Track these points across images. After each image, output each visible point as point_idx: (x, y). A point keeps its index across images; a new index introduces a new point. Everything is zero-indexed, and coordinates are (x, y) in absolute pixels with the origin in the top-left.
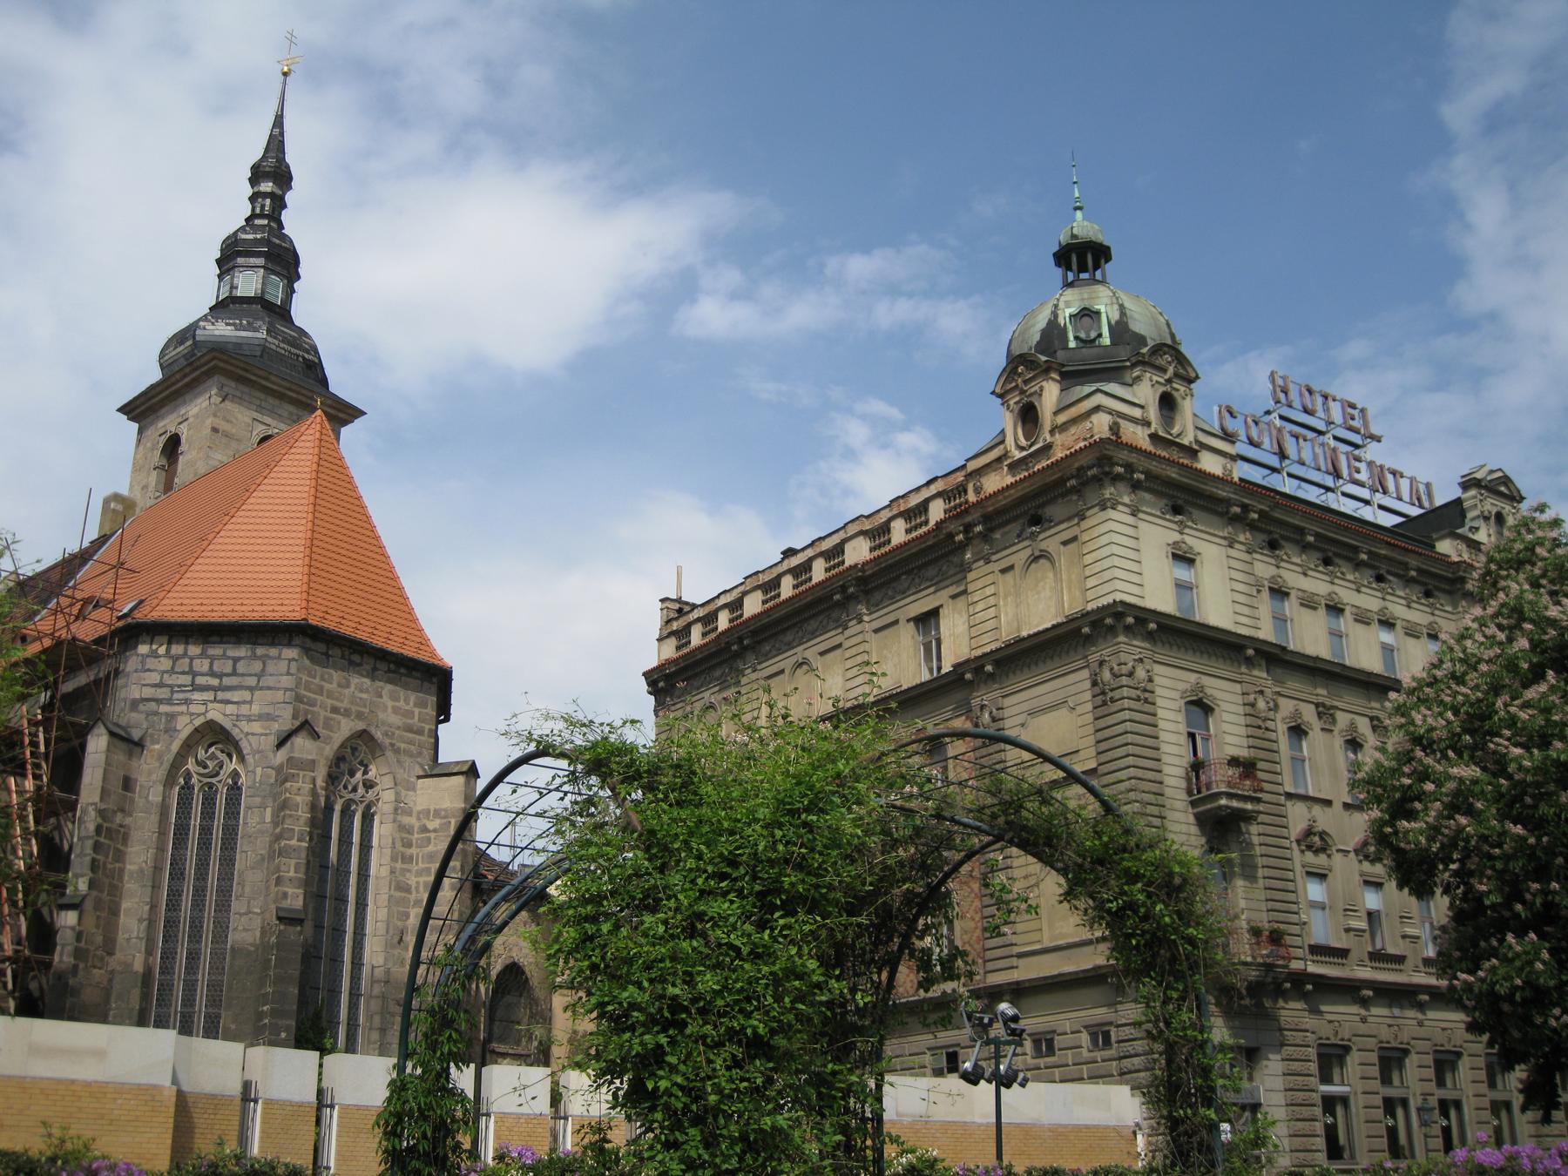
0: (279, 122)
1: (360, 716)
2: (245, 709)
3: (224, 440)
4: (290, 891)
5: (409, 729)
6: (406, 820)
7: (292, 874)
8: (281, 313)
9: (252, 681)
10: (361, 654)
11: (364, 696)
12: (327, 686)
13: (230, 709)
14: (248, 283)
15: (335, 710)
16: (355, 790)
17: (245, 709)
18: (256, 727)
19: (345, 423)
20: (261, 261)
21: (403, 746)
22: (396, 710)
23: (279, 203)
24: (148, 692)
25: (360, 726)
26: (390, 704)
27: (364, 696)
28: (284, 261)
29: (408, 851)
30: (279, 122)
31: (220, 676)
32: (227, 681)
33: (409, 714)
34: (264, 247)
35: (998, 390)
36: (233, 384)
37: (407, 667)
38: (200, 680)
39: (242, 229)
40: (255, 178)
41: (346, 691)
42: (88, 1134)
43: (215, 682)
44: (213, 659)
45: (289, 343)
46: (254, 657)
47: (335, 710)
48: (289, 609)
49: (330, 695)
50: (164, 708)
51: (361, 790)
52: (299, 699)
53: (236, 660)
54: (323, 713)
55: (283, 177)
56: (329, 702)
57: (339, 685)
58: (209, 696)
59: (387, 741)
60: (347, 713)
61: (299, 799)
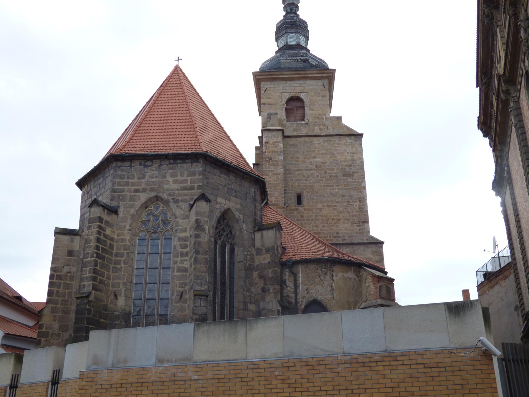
1: (152, 190)
3: (269, 106)
4: (86, 283)
7: (88, 275)
10: (151, 160)
11: (154, 180)
12: (131, 181)
15: (136, 191)
21: (180, 198)
22: (175, 182)
26: (171, 180)
27: (154, 180)
34: (292, 25)
36: (269, 83)
37: (180, 159)
41: (143, 180)
45: (292, 56)
49: (133, 184)
54: (129, 194)
56: (133, 188)
57: (139, 178)
59: (170, 198)
60: (144, 190)
61: (92, 237)
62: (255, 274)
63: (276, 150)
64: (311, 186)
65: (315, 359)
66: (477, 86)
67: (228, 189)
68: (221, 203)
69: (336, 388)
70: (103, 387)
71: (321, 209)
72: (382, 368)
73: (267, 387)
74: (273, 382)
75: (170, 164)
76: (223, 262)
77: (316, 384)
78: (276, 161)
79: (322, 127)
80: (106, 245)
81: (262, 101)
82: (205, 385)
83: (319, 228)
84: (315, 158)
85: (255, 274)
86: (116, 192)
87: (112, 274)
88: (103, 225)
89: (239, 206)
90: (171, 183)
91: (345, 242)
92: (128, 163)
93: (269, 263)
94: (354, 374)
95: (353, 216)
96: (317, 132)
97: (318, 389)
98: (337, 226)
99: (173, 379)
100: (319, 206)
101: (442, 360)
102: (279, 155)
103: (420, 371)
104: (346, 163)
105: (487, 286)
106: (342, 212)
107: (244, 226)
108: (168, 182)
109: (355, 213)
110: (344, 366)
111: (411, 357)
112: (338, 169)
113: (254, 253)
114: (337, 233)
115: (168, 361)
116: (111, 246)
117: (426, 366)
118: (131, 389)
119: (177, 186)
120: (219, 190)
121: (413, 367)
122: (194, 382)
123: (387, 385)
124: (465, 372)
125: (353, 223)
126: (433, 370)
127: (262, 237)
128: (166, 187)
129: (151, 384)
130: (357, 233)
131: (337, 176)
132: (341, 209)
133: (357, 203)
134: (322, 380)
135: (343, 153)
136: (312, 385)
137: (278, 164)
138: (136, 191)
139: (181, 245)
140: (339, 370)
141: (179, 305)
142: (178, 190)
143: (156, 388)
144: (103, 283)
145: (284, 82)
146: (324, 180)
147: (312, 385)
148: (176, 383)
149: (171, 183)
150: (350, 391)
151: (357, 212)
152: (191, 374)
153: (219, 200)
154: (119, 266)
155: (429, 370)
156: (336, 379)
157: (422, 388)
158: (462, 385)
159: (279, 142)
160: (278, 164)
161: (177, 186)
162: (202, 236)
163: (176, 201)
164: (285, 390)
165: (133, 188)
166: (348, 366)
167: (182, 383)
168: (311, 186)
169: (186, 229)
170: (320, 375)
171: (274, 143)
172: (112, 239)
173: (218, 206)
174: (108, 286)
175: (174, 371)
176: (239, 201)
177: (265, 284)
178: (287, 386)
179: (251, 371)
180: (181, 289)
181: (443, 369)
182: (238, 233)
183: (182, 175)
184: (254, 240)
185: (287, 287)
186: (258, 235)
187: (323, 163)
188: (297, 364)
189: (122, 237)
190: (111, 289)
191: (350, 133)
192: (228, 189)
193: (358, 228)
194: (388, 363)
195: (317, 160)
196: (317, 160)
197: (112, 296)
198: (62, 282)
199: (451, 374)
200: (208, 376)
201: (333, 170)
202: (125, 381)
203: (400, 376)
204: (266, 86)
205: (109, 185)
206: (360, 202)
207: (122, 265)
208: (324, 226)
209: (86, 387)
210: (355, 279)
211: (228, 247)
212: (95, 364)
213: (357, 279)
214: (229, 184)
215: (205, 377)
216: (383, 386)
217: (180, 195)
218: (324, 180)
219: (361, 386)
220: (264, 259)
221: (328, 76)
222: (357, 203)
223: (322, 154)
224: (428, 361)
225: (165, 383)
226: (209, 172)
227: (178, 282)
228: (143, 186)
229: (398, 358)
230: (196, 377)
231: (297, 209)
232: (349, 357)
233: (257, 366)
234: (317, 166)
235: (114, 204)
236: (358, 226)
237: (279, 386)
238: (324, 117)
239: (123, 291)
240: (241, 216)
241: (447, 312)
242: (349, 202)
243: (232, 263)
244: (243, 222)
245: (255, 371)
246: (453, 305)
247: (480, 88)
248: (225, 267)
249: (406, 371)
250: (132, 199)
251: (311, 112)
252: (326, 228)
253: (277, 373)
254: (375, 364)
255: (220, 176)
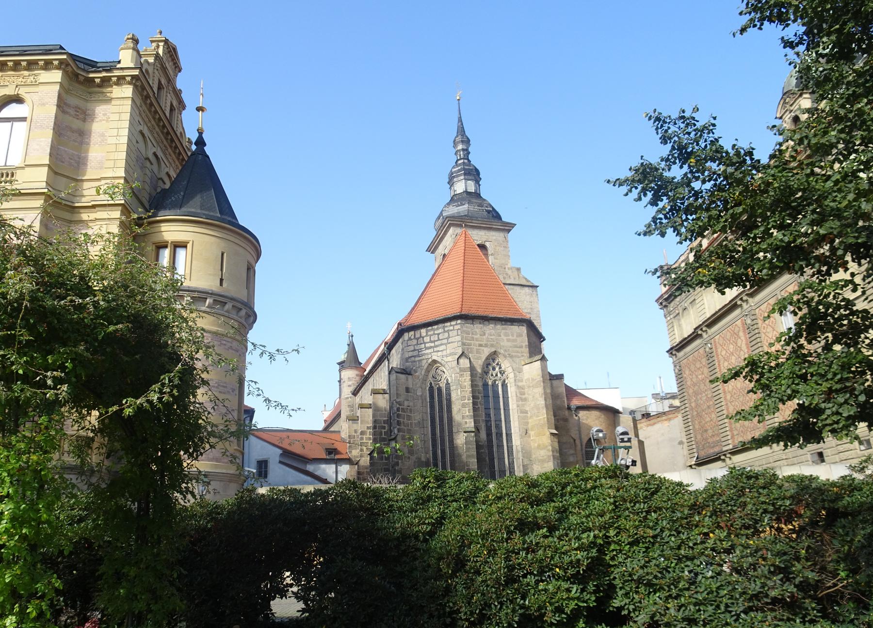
0: (460, 120)
1: (492, 346)
2: (444, 353)
5: (516, 347)
6: (520, 384)
8: (477, 195)
9: (445, 341)
12: (475, 337)
13: (440, 354)
14: (460, 187)
15: (480, 345)
16: (497, 375)
17: (444, 353)
18: (449, 359)
19: (509, 231)
20: (462, 177)
22: (508, 340)
23: (467, 152)
24: (411, 354)
25: (493, 350)
26: (505, 338)
28: (473, 174)
29: (524, 397)
30: (460, 120)
31: (434, 341)
32: (436, 343)
33: (515, 341)
35: (778, 116)
38: (427, 345)
39: (454, 167)
40: (455, 144)
42: (789, 449)
43: (432, 345)
44: (430, 336)
46: (445, 331)
47: (480, 345)
48: (455, 310)
50: (417, 359)
51: (499, 375)
52: (463, 344)
53: (438, 334)
55: (467, 141)
58: (432, 350)
60: (486, 346)
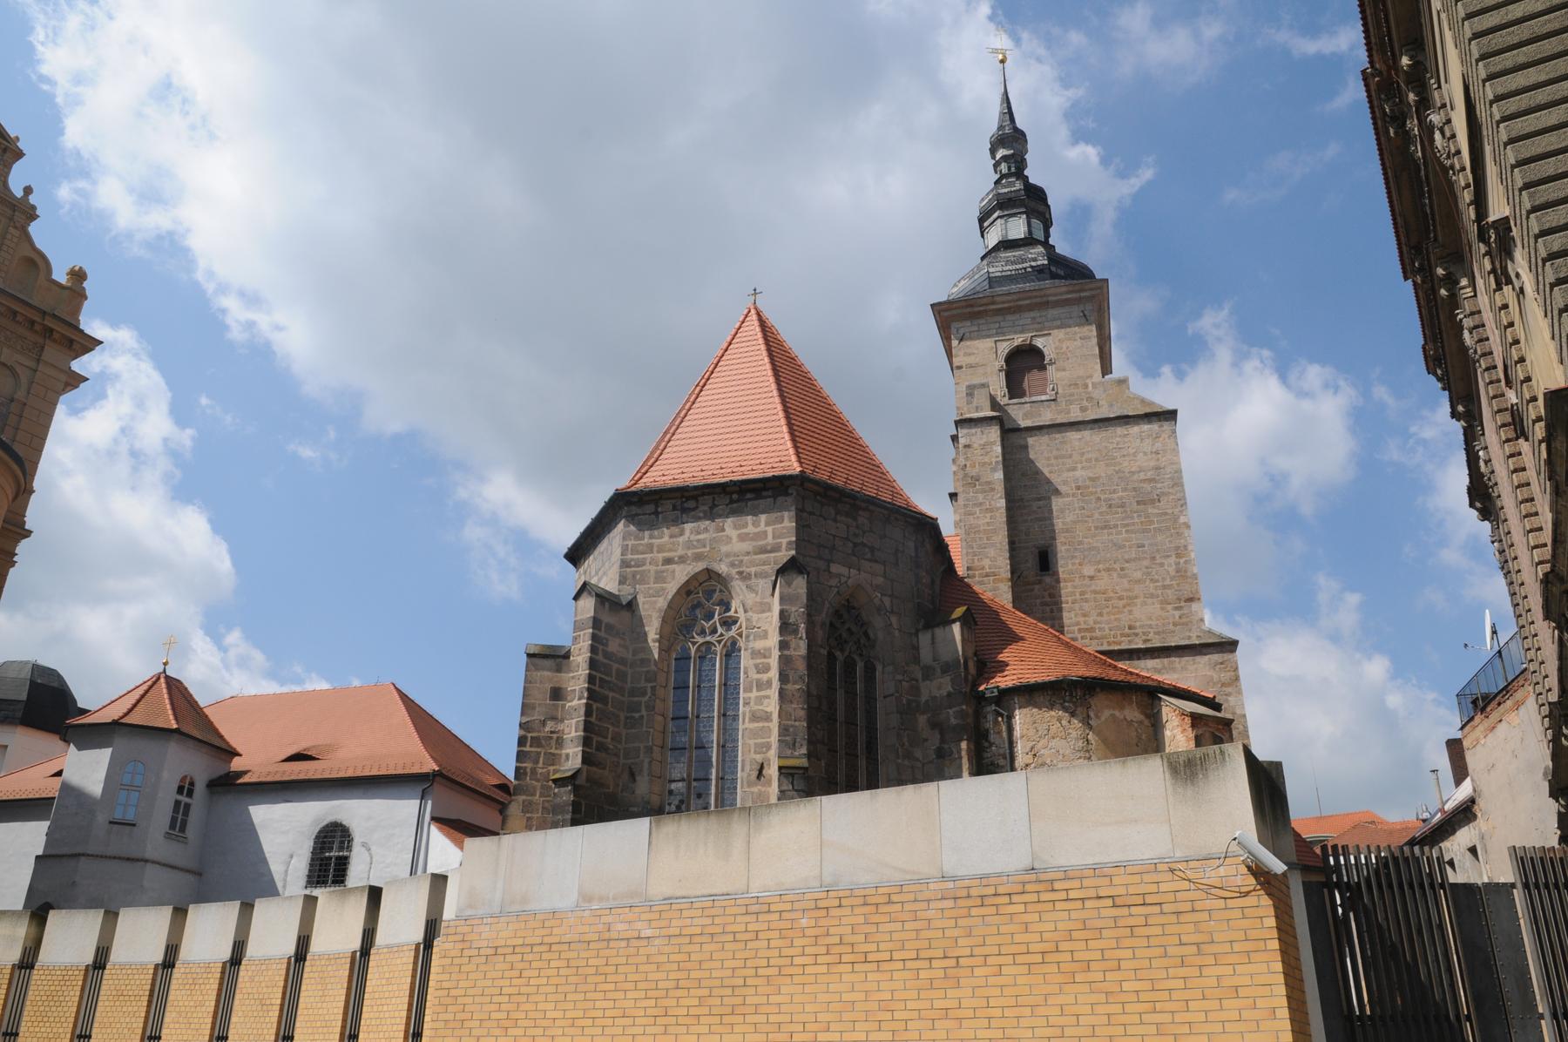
7: (573, 734)
11: (701, 537)
15: (668, 561)
21: (753, 570)
22: (742, 538)
27: (701, 537)
41: (681, 539)
54: (653, 568)
56: (661, 556)
60: (683, 560)
62: (922, 720)
63: (986, 459)
64: (1067, 531)
65: (881, 891)
66: (1406, 278)
67: (855, 545)
68: (839, 575)
69: (923, 954)
70: (482, 952)
71: (1092, 578)
72: (1021, 908)
73: (785, 952)
74: (797, 942)
75: (732, 501)
76: (851, 693)
77: (882, 946)
78: (989, 483)
79: (1085, 403)
80: (609, 674)
81: (956, 361)
82: (666, 949)
83: (1091, 621)
84: (1074, 469)
85: (922, 720)
86: (629, 566)
87: (624, 732)
88: (602, 634)
89: (880, 580)
90: (735, 539)
91: (1149, 645)
92: (650, 508)
93: (949, 694)
94: (961, 922)
95: (1164, 587)
96: (1075, 415)
97: (887, 956)
98: (1130, 612)
99: (607, 936)
100: (1088, 570)
101: (1154, 888)
102: (994, 470)
103: (1104, 913)
104: (1142, 476)
105: (1481, 728)
106: (1138, 581)
107: (894, 620)
108: (729, 539)
109: (1168, 582)
110: (941, 904)
111: (1086, 883)
112: (1125, 490)
113: (919, 676)
114: (1130, 628)
115: (601, 899)
116: (622, 676)
117: (1119, 901)
118: (530, 957)
119: (746, 546)
120: (834, 547)
121: (1088, 904)
122: (645, 943)
123: (1033, 948)
124: (1205, 916)
125: (1165, 602)
126: (1134, 910)
127: (933, 638)
128: (724, 549)
129: (566, 947)
130: (1175, 624)
131: (1123, 506)
132: (1138, 575)
133: (1173, 560)
134: (895, 936)
135: (1135, 454)
136: (873, 947)
137: (993, 490)
138: (668, 561)
139: (756, 666)
140: (930, 914)
141: (755, 789)
142: (748, 553)
143: (574, 955)
144: (606, 750)
145: (999, 318)
146: (1097, 516)
147: (873, 947)
148: (612, 944)
149: (735, 539)
150: (952, 962)
151: (1172, 578)
152: (639, 925)
153: (835, 568)
154: (637, 715)
155: (1125, 911)
156: (924, 934)
157: (1108, 954)
158: (1197, 944)
159: (993, 443)
160: (993, 490)
161: (746, 546)
162: (793, 645)
163: (744, 577)
164: (820, 960)
165: (661, 556)
166: (950, 903)
167: (624, 944)
168: (1067, 531)
169: (766, 632)
170: (892, 926)
171: (983, 446)
172: (623, 661)
173: (834, 582)
174: (616, 755)
175: (610, 919)
176: (879, 568)
177: (943, 741)
178: (823, 950)
179: (752, 918)
180: (759, 758)
181: (1157, 909)
182: (880, 635)
183: (756, 524)
184: (916, 648)
185: (991, 745)
186: (924, 639)
187: (1092, 479)
188: (844, 902)
189: (642, 656)
190: (622, 761)
191: (1148, 410)
192: (855, 545)
193: (1177, 613)
194: (1034, 897)
195: (1078, 473)
196: (1078, 473)
197: (626, 776)
198: (542, 751)
199: (1173, 918)
200: (672, 931)
201: (1114, 491)
202: (520, 941)
203: (1060, 926)
204: (962, 331)
205: (618, 552)
206: (1178, 556)
207: (644, 713)
208: (1100, 614)
209: (453, 953)
210: (1141, 722)
211: (860, 666)
212: (470, 906)
213: (1147, 722)
214: (856, 535)
215: (664, 932)
216: (1023, 949)
217: (753, 563)
218: (1097, 516)
219: (977, 951)
220: (939, 688)
221: (1093, 296)
222: (1173, 560)
223: (1089, 460)
224: (1122, 891)
225: (592, 945)
226: (811, 513)
227: (752, 742)
228: (680, 552)
229: (1057, 886)
230: (649, 933)
231: (1040, 582)
232: (951, 885)
233: (765, 908)
234: (1078, 488)
235: (625, 593)
236: (1176, 609)
237: (807, 951)
238: (1089, 382)
239: (646, 765)
240: (887, 601)
241: (1168, 775)
242: (1154, 558)
243: (870, 699)
244: (892, 612)
245: (761, 917)
246: (1181, 760)
247: (1415, 284)
248: (855, 709)
249: (1074, 915)
250: (660, 578)
251: (1060, 374)
252: (1105, 618)
253: (804, 922)
254: (1006, 899)
255: (835, 520)
